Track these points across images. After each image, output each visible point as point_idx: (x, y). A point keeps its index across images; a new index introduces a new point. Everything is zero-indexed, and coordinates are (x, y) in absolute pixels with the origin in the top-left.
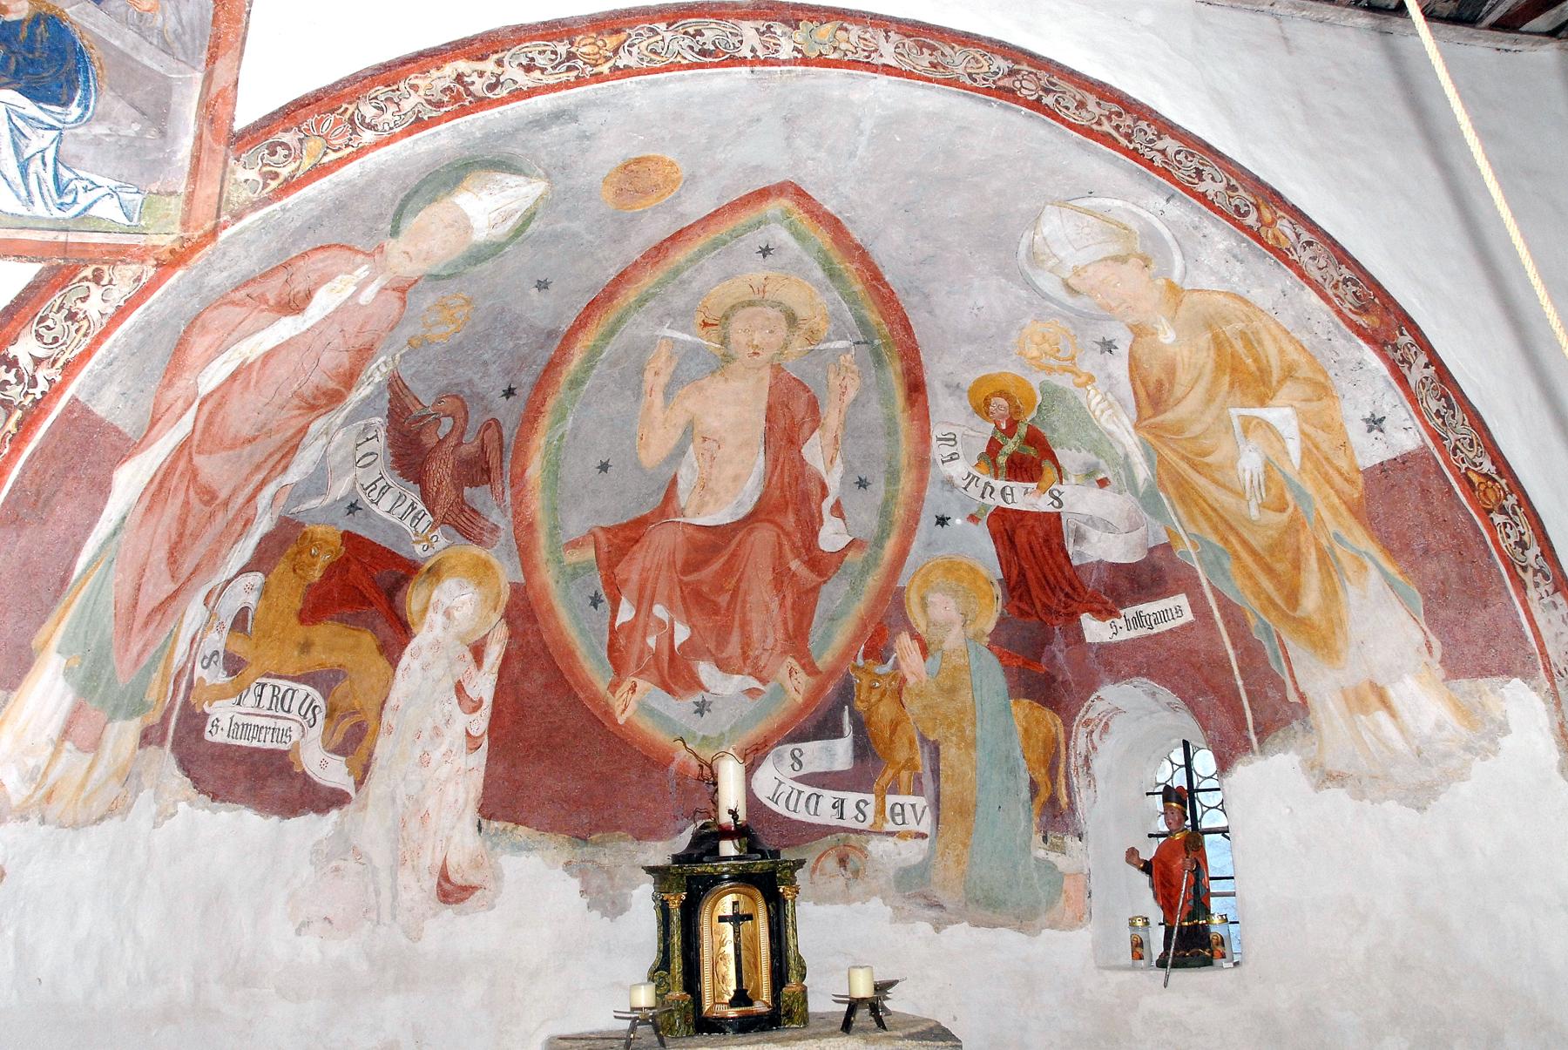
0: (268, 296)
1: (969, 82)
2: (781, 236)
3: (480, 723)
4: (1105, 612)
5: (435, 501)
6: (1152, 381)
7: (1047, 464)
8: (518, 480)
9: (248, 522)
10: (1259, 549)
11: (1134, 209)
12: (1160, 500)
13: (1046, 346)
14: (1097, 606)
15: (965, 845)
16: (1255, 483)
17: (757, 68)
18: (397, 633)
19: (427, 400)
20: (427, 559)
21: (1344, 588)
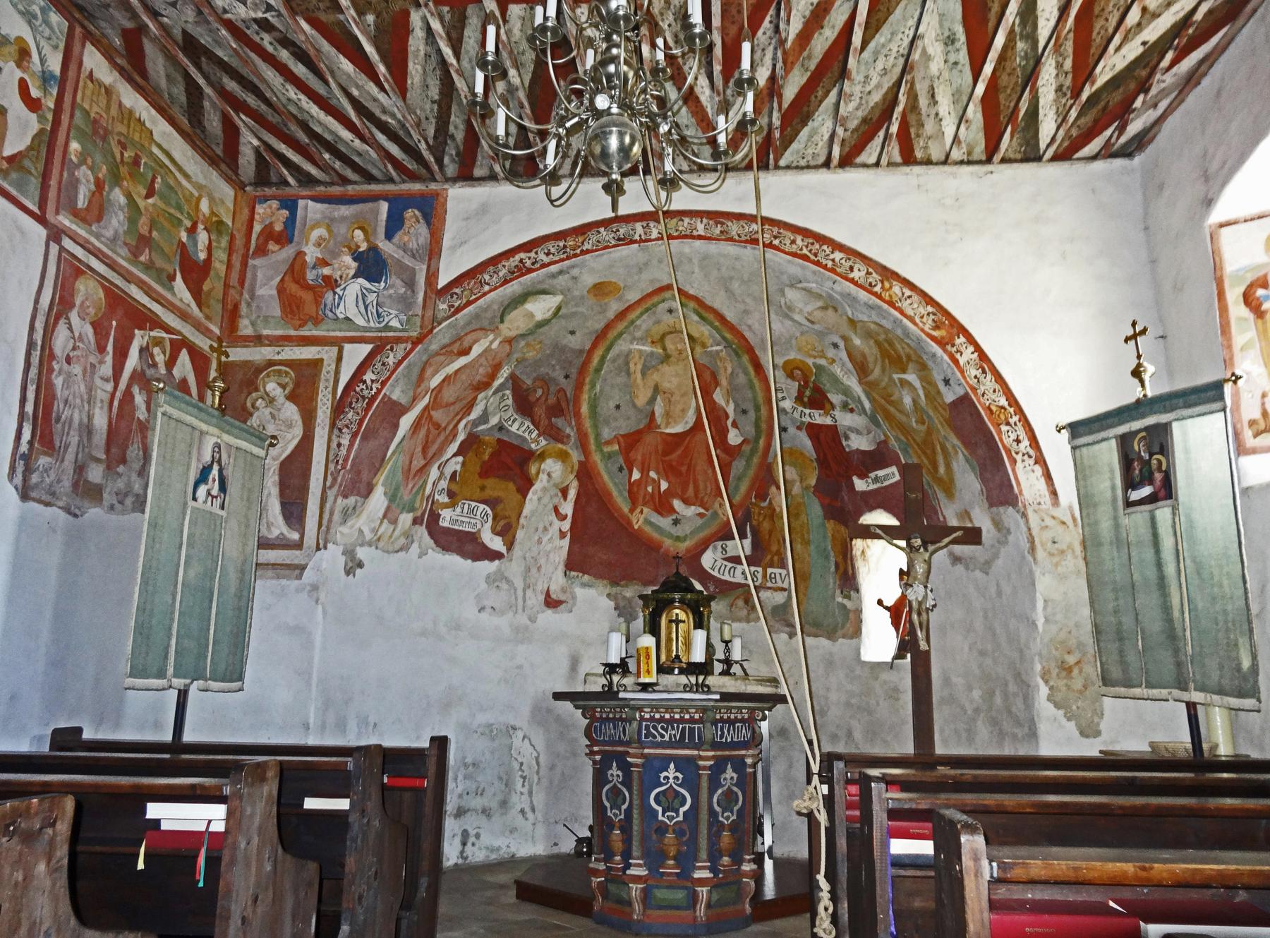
3: (566, 526)
4: (863, 476)
8: (577, 414)
9: (455, 436)
18: (525, 484)
19: (529, 382)
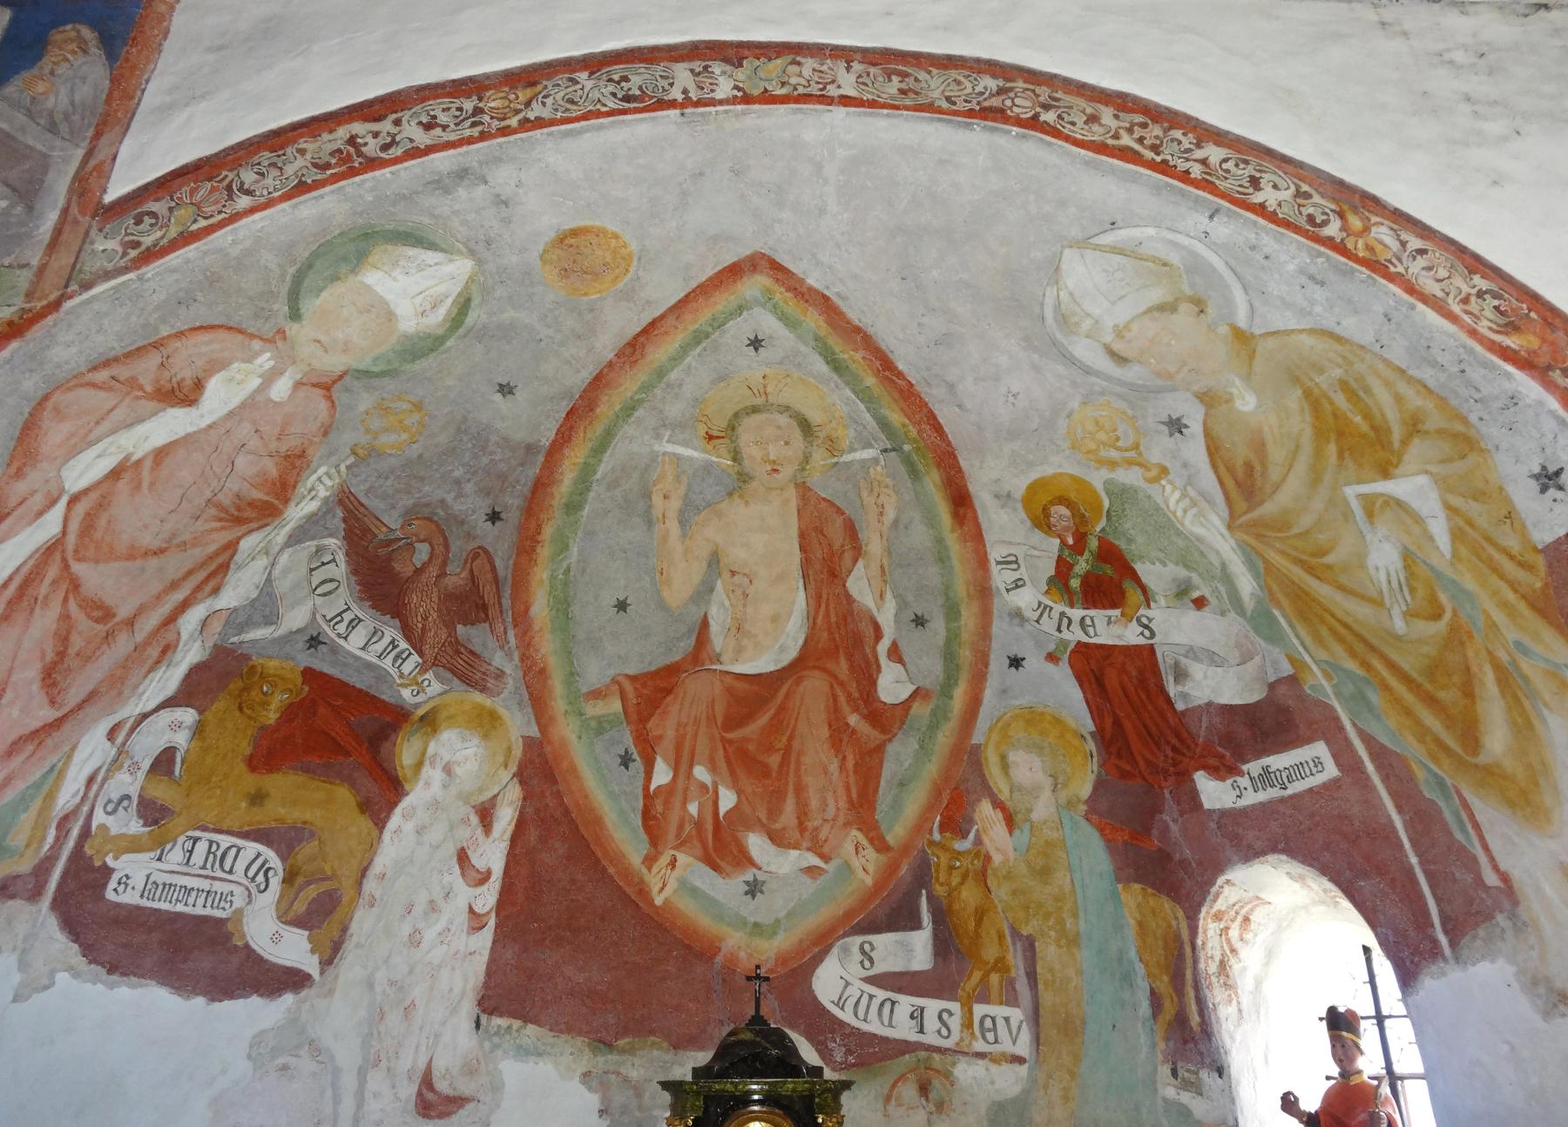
0: (142, 381)
1: (945, 105)
2: (768, 324)
4: (1224, 769)
5: (422, 639)
6: (1239, 463)
7: (1128, 585)
8: (522, 618)
9: (167, 650)
10: (1415, 675)
11: (1170, 236)
12: (1274, 619)
13: (1102, 436)
14: (1212, 761)
15: (1073, 1075)
16: (1395, 584)
17: (689, 111)
18: (383, 790)
20: (417, 706)
21: (1544, 721)
